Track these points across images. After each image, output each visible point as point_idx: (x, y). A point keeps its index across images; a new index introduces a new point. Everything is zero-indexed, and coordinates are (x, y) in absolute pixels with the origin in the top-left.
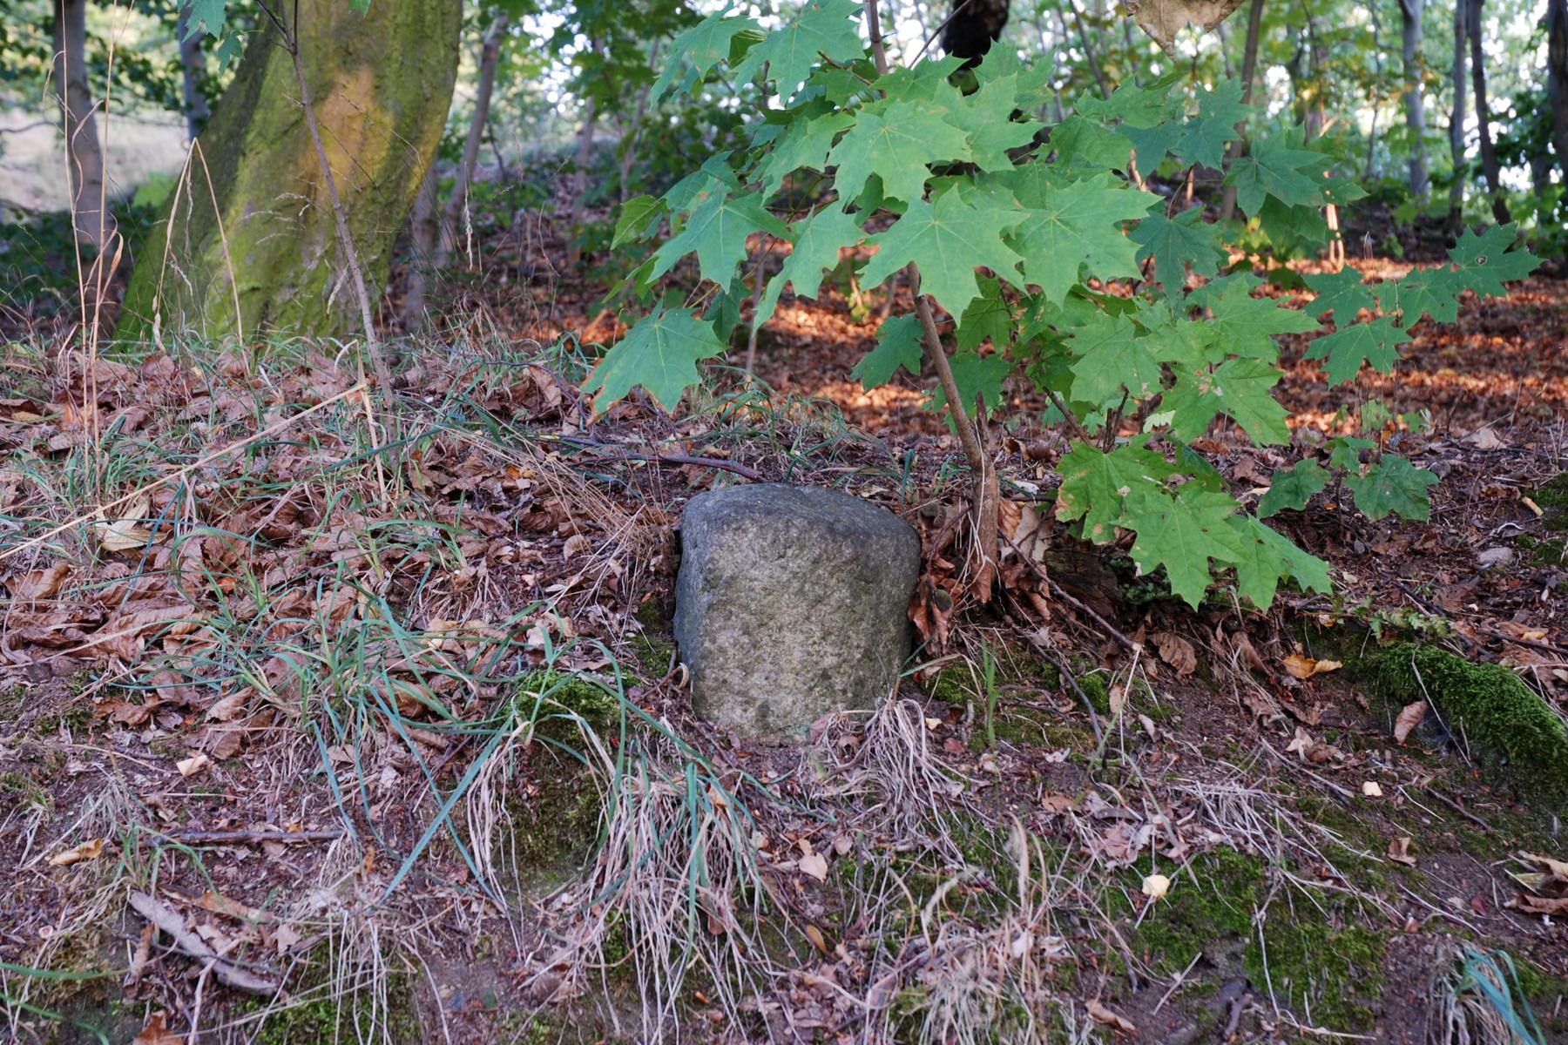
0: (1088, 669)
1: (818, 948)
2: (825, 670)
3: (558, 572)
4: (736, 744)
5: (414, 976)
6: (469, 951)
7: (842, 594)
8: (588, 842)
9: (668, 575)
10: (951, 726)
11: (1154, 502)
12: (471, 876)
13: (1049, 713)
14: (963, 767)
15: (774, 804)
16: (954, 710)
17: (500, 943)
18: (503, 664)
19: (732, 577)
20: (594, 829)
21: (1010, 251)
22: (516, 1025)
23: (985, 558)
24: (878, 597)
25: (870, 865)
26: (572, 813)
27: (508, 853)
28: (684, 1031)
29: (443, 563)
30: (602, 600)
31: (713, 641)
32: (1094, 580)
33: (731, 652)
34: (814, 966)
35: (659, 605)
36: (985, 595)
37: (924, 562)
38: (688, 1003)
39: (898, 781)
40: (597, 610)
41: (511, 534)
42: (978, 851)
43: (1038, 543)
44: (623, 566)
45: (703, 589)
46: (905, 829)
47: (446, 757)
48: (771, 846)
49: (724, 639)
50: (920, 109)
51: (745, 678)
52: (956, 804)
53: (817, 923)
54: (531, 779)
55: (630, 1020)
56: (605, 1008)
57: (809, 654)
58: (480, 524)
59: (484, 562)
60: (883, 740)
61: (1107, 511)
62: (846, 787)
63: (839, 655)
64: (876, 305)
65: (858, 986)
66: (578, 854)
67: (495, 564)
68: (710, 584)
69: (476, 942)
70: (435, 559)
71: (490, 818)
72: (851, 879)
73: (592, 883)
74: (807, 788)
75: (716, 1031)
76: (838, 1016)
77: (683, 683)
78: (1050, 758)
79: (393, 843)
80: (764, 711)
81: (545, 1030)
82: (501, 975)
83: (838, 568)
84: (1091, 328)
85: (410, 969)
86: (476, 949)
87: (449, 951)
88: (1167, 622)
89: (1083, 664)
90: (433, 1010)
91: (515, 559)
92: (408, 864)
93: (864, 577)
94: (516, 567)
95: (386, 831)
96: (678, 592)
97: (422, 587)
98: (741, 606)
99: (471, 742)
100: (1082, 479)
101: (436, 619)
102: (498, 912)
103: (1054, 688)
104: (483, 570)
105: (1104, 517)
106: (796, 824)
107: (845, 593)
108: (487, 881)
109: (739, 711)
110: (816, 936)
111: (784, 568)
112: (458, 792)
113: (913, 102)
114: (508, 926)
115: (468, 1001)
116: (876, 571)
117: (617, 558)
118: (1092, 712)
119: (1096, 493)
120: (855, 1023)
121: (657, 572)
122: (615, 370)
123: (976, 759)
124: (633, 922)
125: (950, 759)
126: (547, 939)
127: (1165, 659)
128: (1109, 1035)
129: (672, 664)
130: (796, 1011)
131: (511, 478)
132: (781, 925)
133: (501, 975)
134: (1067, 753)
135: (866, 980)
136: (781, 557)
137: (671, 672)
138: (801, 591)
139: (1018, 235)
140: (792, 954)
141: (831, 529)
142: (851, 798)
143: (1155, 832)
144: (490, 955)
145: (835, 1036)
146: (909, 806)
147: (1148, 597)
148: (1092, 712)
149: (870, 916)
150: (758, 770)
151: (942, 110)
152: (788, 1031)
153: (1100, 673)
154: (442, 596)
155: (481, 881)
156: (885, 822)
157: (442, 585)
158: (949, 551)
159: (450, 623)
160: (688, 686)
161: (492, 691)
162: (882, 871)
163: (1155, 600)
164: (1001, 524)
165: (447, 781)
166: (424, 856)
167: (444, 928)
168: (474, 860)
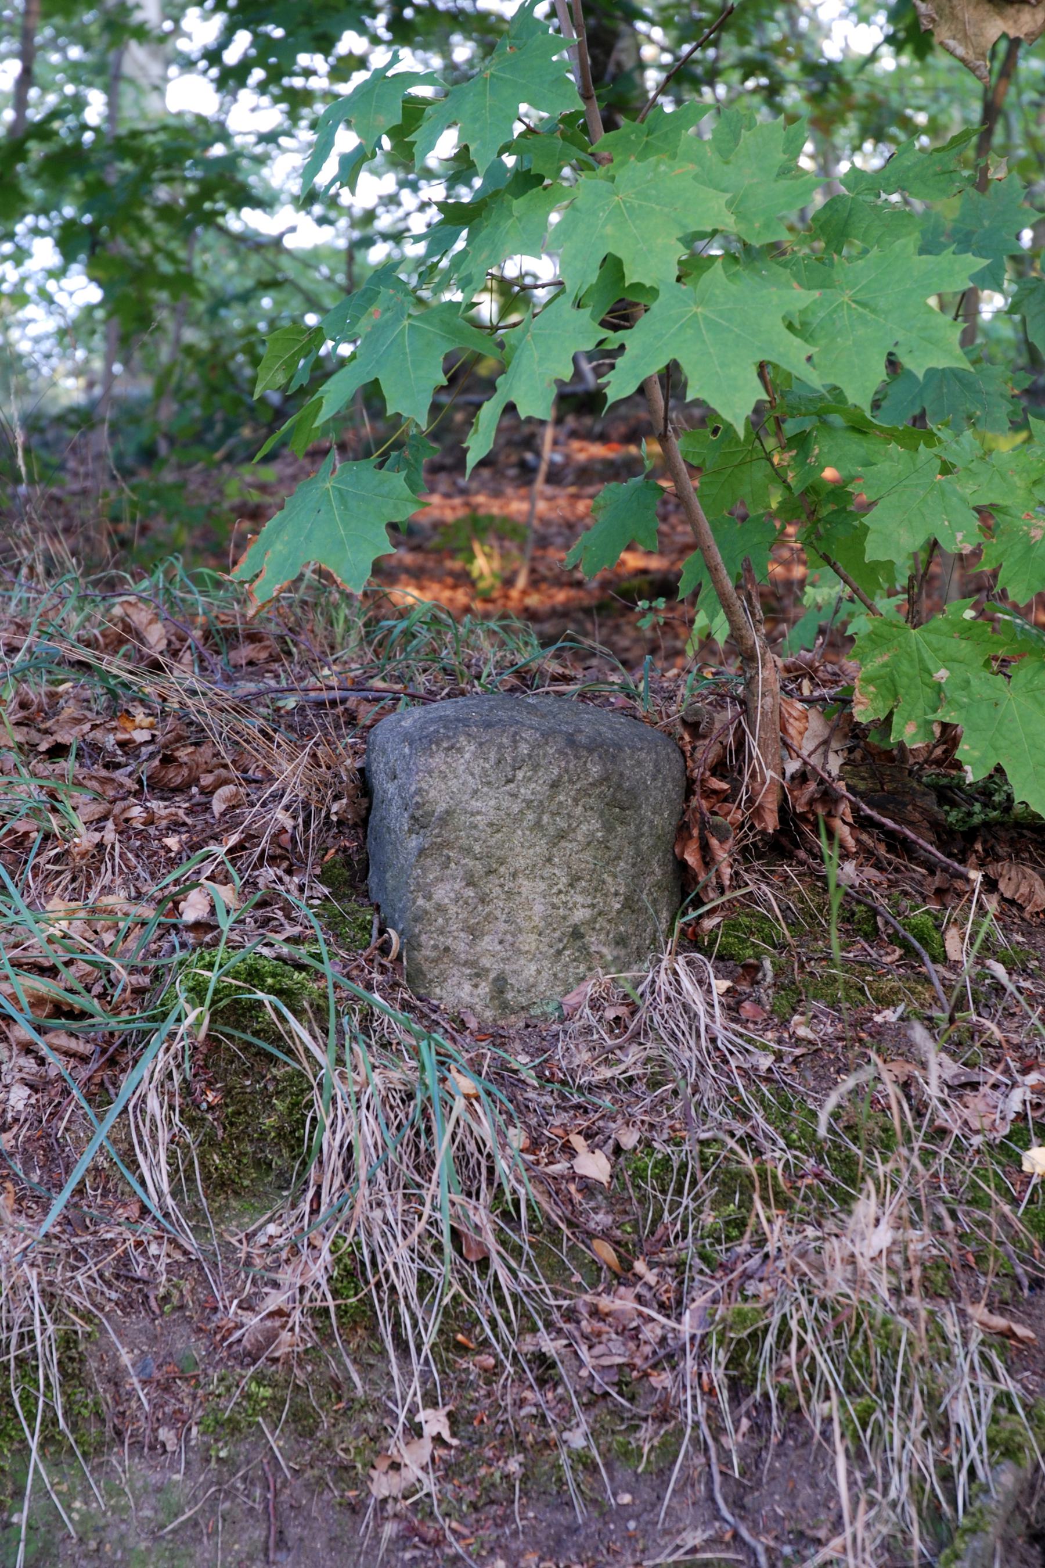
0: (913, 910)
1: (609, 1268)
2: (576, 927)
3: (209, 832)
4: (473, 1024)
5: (88, 1336)
6: (153, 1303)
7: (591, 826)
8: (294, 1158)
9: (355, 825)
10: (744, 987)
11: (985, 684)
12: (144, 1211)
13: (869, 965)
14: (769, 1035)
15: (531, 1094)
16: (747, 967)
17: (193, 1291)
18: (154, 947)
19: (447, 812)
20: (300, 1140)
21: (797, 341)
22: (228, 1389)
23: (769, 774)
24: (638, 828)
25: (667, 1159)
26: (269, 1122)
27: (190, 1179)
28: (446, 1385)
29: (57, 830)
30: (273, 860)
31: (428, 897)
32: (907, 799)
33: (453, 909)
34: (608, 1290)
35: (348, 863)
36: (771, 823)
37: (690, 782)
38: (447, 1350)
39: (688, 1055)
40: (268, 873)
41: (137, 794)
42: (802, 1135)
43: (832, 756)
44: (295, 818)
45: (410, 831)
46: (706, 1114)
47: (93, 1066)
48: (534, 1145)
49: (442, 893)
50: (662, 168)
51: (472, 944)
52: (767, 1080)
53: (606, 1235)
54: (210, 1084)
55: (374, 1376)
56: (340, 1363)
57: (554, 906)
58: (95, 784)
59: (110, 825)
60: (664, 1006)
61: (921, 704)
62: (623, 1067)
63: (593, 906)
64: (507, 573)
65: (673, 1308)
66: (281, 1174)
67: (124, 828)
68: (419, 823)
69: (162, 1291)
70: (45, 824)
71: (164, 1136)
72: (644, 1179)
73: (305, 1207)
74: (572, 1072)
75: (489, 1382)
76: (647, 1350)
77: (393, 954)
78: (878, 1019)
79: (35, 1178)
80: (500, 985)
81: (267, 1392)
82: (200, 1330)
83: (583, 792)
84: (884, 467)
85: (81, 1327)
86: (166, 1299)
87: (127, 1305)
88: (1002, 850)
89: (906, 903)
90: (115, 1380)
91: (150, 822)
92: (59, 1203)
93: (618, 802)
94: (152, 831)
95: (24, 1164)
96: (371, 845)
97: (31, 862)
98: (461, 848)
99: (124, 1044)
100: (885, 665)
101: (56, 900)
102: (186, 1253)
103: (872, 935)
104: (110, 835)
105: (919, 712)
106: (564, 1117)
107: (595, 824)
108: (166, 1215)
109: (467, 987)
110: (606, 1252)
111: (514, 796)
112: (116, 1108)
113: (653, 159)
114: (201, 1269)
115: (159, 1367)
116: (632, 793)
117: (287, 808)
118: (927, 958)
119: (905, 681)
120: (670, 1357)
121: (340, 823)
122: (278, 547)
123: (785, 1023)
124: (366, 1251)
125: (751, 1026)
126: (254, 1282)
127: (1008, 895)
128: (1003, 1346)
129: (375, 933)
130: (590, 1348)
131: (125, 730)
132: (558, 1244)
133: (200, 1330)
134: (900, 1009)
135: (679, 1302)
136: (509, 781)
137: (375, 941)
138: (538, 825)
139: (803, 324)
140: (577, 1278)
141: (571, 741)
142: (631, 1080)
143: (1029, 1096)
144: (182, 1307)
145: (646, 1375)
146: (706, 1085)
147: (977, 820)
148: (927, 958)
149: (674, 1223)
150: (510, 1046)
151: (691, 168)
152: (584, 1373)
153: (927, 912)
154: (59, 873)
155: (159, 1215)
156: (678, 1107)
157: (57, 859)
158: (719, 769)
159: (73, 905)
160: (399, 958)
161: (145, 980)
162: (684, 1166)
163: (985, 824)
164: (784, 729)
165: (99, 1095)
166: (80, 1191)
167: (117, 1277)
168: (146, 1190)
